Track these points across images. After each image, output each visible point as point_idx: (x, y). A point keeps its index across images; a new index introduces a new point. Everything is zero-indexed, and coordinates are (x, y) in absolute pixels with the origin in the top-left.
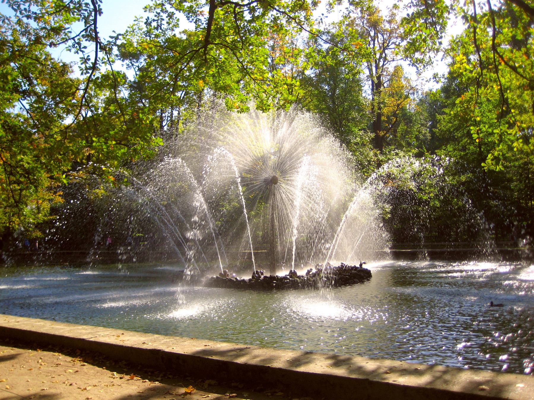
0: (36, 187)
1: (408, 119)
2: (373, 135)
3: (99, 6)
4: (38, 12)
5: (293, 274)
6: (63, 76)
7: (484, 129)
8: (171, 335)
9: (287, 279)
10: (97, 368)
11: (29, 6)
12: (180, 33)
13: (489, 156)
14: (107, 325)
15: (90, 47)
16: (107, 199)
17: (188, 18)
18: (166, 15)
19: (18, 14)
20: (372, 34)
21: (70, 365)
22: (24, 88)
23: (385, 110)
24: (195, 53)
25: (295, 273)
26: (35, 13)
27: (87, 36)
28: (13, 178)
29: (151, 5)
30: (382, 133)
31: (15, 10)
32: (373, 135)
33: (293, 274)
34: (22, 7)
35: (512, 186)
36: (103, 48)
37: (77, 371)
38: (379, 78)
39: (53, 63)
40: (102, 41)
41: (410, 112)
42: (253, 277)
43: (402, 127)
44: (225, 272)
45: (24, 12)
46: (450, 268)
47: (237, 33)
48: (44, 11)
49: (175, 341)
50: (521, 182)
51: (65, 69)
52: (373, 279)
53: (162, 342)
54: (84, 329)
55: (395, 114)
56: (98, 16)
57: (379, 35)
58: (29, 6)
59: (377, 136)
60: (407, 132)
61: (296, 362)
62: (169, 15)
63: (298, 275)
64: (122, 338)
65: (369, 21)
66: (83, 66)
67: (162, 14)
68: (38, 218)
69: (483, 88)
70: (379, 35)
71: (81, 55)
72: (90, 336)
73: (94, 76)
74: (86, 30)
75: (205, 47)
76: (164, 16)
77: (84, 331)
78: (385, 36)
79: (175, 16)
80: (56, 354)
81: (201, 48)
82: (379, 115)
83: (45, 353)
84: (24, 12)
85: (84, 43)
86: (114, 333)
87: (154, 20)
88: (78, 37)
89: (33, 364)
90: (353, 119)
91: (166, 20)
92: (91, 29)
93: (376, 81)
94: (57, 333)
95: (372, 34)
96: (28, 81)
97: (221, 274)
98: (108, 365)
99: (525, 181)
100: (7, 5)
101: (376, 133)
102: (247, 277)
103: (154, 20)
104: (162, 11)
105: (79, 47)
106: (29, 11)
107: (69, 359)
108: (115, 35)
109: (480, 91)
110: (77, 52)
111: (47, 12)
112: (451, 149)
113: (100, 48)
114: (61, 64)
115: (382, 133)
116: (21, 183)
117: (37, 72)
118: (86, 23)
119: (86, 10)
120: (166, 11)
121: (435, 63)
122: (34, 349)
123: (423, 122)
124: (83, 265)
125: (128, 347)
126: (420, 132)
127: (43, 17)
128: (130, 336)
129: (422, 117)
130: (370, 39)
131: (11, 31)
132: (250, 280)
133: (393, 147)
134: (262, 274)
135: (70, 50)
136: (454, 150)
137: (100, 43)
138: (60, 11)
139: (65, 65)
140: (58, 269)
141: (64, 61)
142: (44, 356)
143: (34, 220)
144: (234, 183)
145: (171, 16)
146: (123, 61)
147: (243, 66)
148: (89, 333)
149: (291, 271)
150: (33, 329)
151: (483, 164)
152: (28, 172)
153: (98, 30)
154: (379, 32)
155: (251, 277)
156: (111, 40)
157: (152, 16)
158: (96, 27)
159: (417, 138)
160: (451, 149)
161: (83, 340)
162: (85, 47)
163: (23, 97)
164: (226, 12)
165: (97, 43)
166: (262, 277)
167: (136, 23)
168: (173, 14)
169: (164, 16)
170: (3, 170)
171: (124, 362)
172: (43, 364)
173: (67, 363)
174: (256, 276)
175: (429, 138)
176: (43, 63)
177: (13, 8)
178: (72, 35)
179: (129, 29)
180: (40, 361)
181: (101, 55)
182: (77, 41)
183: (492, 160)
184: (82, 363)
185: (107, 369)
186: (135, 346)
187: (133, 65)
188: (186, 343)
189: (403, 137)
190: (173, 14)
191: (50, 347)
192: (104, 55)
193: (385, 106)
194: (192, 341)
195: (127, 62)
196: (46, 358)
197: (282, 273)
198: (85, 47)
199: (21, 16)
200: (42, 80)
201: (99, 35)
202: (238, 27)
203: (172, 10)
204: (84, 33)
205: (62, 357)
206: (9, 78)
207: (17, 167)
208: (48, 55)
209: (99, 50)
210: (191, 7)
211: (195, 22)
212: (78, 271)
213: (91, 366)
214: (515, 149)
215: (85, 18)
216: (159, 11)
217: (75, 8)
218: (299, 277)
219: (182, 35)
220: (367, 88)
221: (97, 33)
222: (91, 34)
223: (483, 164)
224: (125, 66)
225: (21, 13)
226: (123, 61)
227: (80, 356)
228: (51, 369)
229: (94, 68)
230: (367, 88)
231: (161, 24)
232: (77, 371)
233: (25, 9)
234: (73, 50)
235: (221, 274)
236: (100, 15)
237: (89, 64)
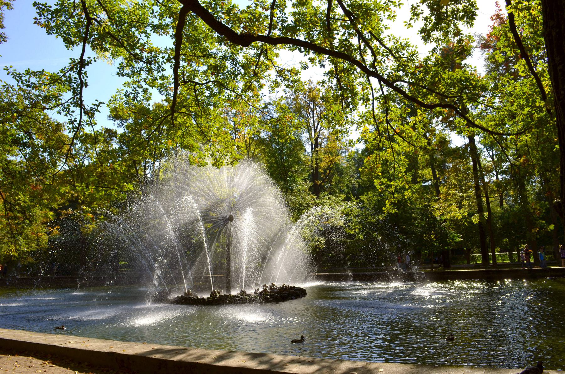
0: (30, 222)
1: (340, 171)
2: (310, 184)
3: (86, 80)
4: (36, 83)
5: (243, 293)
6: (57, 133)
7: (384, 182)
8: (128, 341)
9: (239, 297)
10: (62, 369)
11: (29, 78)
12: (162, 101)
13: (387, 202)
14: (70, 333)
15: (77, 111)
16: (95, 234)
17: (160, 92)
18: (142, 90)
19: (20, 84)
20: (312, 106)
21: (41, 366)
22: (25, 141)
23: (322, 165)
24: (164, 119)
25: (245, 292)
26: (34, 83)
27: (75, 103)
28: (10, 214)
29: (130, 82)
30: (319, 183)
31: (18, 81)
32: (310, 184)
33: (243, 293)
34: (23, 78)
35: (416, 223)
36: (87, 113)
37: (45, 371)
38: (316, 140)
39: (49, 123)
40: (86, 107)
41: (342, 166)
42: (211, 296)
43: (336, 178)
44: (188, 291)
45: (24, 82)
46: (373, 286)
47: (198, 105)
48: (41, 82)
49: (129, 346)
50: (422, 220)
51: (58, 127)
52: (307, 296)
53: (119, 346)
54: (57, 338)
55: (329, 168)
56: (84, 88)
57: (317, 108)
58: (29, 78)
59: (315, 185)
60: (339, 182)
61: (220, 358)
62: (143, 91)
63: (247, 293)
64: (87, 344)
65: (309, 96)
66: (71, 126)
67: (137, 89)
68: (31, 247)
69: (384, 152)
70: (317, 108)
71: (69, 117)
72: (60, 343)
73: (80, 133)
74: (73, 98)
75: (172, 114)
76: (140, 90)
77: (57, 339)
78: (322, 109)
79: (148, 91)
80: (30, 358)
81: (170, 115)
82: (317, 169)
83: (22, 357)
84: (24, 82)
85: (72, 108)
86: (81, 341)
87: (131, 93)
88: (67, 103)
89: (9, 366)
90: (296, 171)
91: (141, 93)
92: (77, 98)
93: (314, 142)
94: (34, 341)
95: (312, 106)
96: (28, 135)
97: (185, 294)
98: (73, 366)
99: (426, 219)
100: (12, 77)
101: (314, 182)
102: (206, 296)
103: (131, 93)
104: (138, 87)
105: (68, 112)
106: (29, 82)
107: (40, 362)
108: (97, 103)
109: (381, 154)
110: (66, 115)
111: (44, 83)
112: (371, 195)
113: (84, 112)
114: (56, 124)
115: (319, 183)
116: (18, 218)
117: (36, 129)
118: (74, 93)
119: (75, 83)
120: (142, 87)
121: (350, 132)
122: (13, 355)
123: (352, 174)
124: (74, 288)
125: (90, 351)
126: (350, 182)
127: (40, 86)
128: (94, 342)
129: (351, 170)
130: (310, 110)
131: (16, 96)
132: (208, 298)
133: (326, 193)
134: (219, 293)
135: (60, 113)
136: (374, 196)
137: (84, 109)
138: (54, 82)
139: (59, 124)
140: (51, 291)
141: (58, 121)
142: (20, 360)
143: (28, 248)
144: (197, 221)
145: (145, 91)
146: (115, 121)
147: (202, 130)
148: (60, 341)
149: (241, 290)
150: (14, 339)
151: (384, 208)
152: (23, 211)
153: (83, 99)
154: (317, 105)
155: (209, 296)
156: (93, 107)
157: (130, 90)
158: (81, 97)
159: (348, 186)
160: (371, 195)
161: (54, 346)
162: (73, 112)
163: (24, 148)
164: (188, 89)
165: (81, 108)
166: (218, 296)
167: (118, 94)
168: (147, 89)
169: (140, 90)
170: (3, 207)
171: (86, 364)
172: (18, 366)
173: (38, 365)
174: (213, 295)
175: (357, 186)
176: (41, 122)
177: (16, 79)
178: (63, 101)
179: (112, 99)
180: (16, 364)
181: (85, 118)
182: (66, 106)
183: (390, 205)
184: (51, 365)
185: (70, 369)
186: (96, 350)
187: (122, 124)
188: (138, 347)
189: (336, 185)
190: (147, 89)
191: (27, 352)
192: (88, 119)
193: (321, 162)
194: (143, 345)
195: (118, 122)
196: (21, 362)
197: (234, 293)
198: (73, 112)
199: (22, 85)
200: (39, 135)
201: (83, 103)
202: (198, 100)
203: (147, 86)
204: (71, 100)
205: (35, 360)
206: (8, 133)
207: (15, 205)
208: (45, 115)
209: (83, 114)
210: (163, 84)
211: (166, 96)
212: (70, 292)
213: (58, 367)
214: (406, 197)
215: (74, 89)
216: (135, 86)
217: (66, 81)
218: (248, 295)
219: (164, 102)
220: (308, 148)
221: (82, 101)
222: (78, 101)
223: (384, 208)
224: (116, 125)
225: (23, 83)
226: (115, 121)
227: (51, 359)
228: (24, 370)
229: (79, 127)
230: (308, 148)
231: (137, 96)
232: (45, 371)
233: (26, 81)
234: (63, 113)
235: (185, 294)
236: (86, 87)
237: (76, 124)
